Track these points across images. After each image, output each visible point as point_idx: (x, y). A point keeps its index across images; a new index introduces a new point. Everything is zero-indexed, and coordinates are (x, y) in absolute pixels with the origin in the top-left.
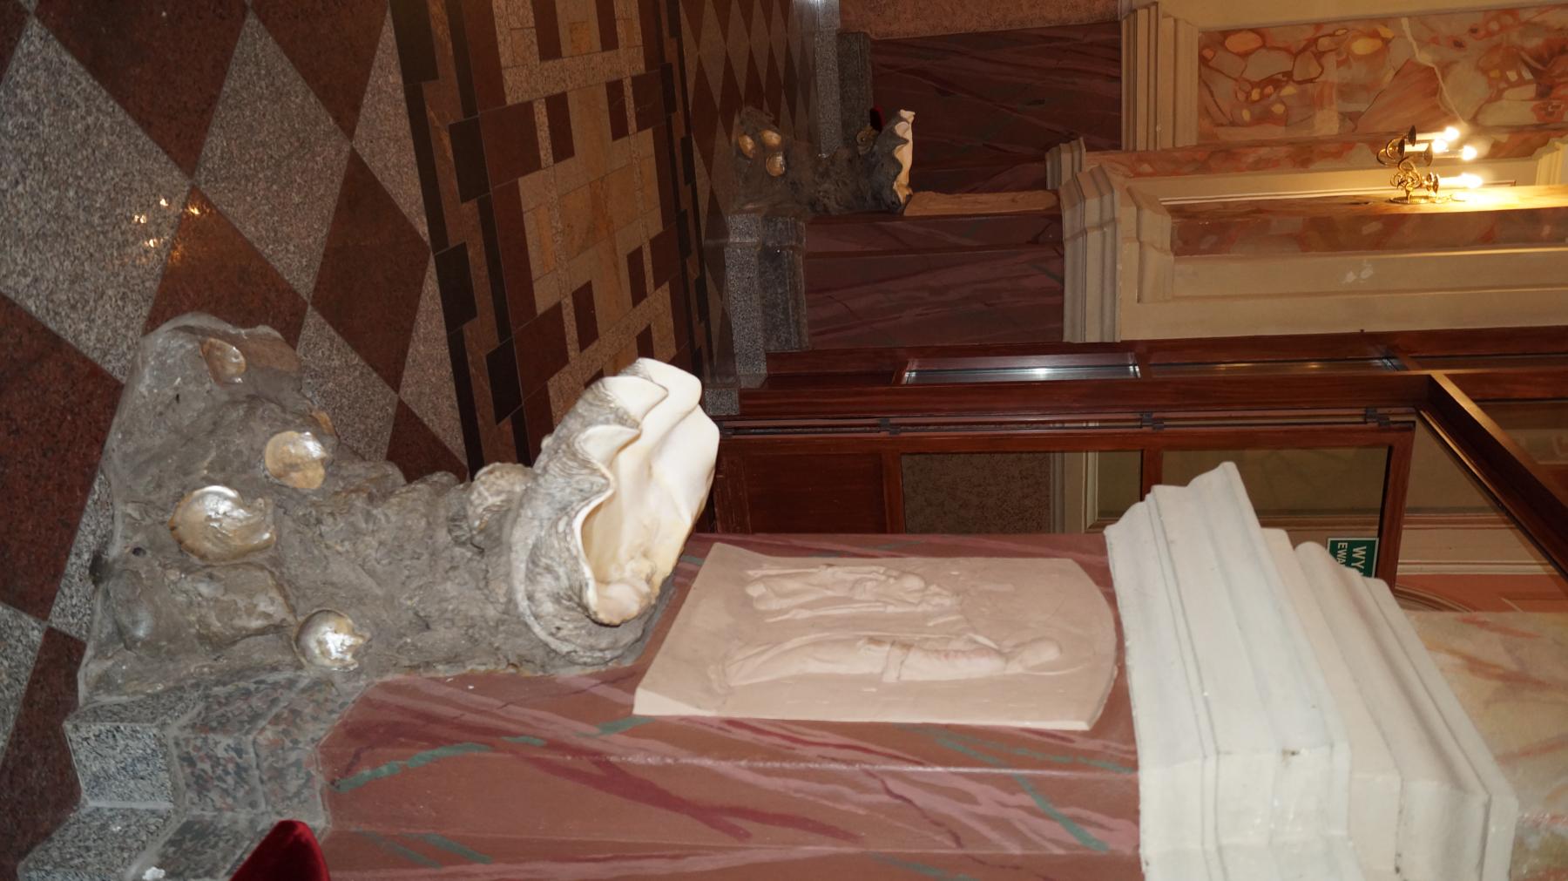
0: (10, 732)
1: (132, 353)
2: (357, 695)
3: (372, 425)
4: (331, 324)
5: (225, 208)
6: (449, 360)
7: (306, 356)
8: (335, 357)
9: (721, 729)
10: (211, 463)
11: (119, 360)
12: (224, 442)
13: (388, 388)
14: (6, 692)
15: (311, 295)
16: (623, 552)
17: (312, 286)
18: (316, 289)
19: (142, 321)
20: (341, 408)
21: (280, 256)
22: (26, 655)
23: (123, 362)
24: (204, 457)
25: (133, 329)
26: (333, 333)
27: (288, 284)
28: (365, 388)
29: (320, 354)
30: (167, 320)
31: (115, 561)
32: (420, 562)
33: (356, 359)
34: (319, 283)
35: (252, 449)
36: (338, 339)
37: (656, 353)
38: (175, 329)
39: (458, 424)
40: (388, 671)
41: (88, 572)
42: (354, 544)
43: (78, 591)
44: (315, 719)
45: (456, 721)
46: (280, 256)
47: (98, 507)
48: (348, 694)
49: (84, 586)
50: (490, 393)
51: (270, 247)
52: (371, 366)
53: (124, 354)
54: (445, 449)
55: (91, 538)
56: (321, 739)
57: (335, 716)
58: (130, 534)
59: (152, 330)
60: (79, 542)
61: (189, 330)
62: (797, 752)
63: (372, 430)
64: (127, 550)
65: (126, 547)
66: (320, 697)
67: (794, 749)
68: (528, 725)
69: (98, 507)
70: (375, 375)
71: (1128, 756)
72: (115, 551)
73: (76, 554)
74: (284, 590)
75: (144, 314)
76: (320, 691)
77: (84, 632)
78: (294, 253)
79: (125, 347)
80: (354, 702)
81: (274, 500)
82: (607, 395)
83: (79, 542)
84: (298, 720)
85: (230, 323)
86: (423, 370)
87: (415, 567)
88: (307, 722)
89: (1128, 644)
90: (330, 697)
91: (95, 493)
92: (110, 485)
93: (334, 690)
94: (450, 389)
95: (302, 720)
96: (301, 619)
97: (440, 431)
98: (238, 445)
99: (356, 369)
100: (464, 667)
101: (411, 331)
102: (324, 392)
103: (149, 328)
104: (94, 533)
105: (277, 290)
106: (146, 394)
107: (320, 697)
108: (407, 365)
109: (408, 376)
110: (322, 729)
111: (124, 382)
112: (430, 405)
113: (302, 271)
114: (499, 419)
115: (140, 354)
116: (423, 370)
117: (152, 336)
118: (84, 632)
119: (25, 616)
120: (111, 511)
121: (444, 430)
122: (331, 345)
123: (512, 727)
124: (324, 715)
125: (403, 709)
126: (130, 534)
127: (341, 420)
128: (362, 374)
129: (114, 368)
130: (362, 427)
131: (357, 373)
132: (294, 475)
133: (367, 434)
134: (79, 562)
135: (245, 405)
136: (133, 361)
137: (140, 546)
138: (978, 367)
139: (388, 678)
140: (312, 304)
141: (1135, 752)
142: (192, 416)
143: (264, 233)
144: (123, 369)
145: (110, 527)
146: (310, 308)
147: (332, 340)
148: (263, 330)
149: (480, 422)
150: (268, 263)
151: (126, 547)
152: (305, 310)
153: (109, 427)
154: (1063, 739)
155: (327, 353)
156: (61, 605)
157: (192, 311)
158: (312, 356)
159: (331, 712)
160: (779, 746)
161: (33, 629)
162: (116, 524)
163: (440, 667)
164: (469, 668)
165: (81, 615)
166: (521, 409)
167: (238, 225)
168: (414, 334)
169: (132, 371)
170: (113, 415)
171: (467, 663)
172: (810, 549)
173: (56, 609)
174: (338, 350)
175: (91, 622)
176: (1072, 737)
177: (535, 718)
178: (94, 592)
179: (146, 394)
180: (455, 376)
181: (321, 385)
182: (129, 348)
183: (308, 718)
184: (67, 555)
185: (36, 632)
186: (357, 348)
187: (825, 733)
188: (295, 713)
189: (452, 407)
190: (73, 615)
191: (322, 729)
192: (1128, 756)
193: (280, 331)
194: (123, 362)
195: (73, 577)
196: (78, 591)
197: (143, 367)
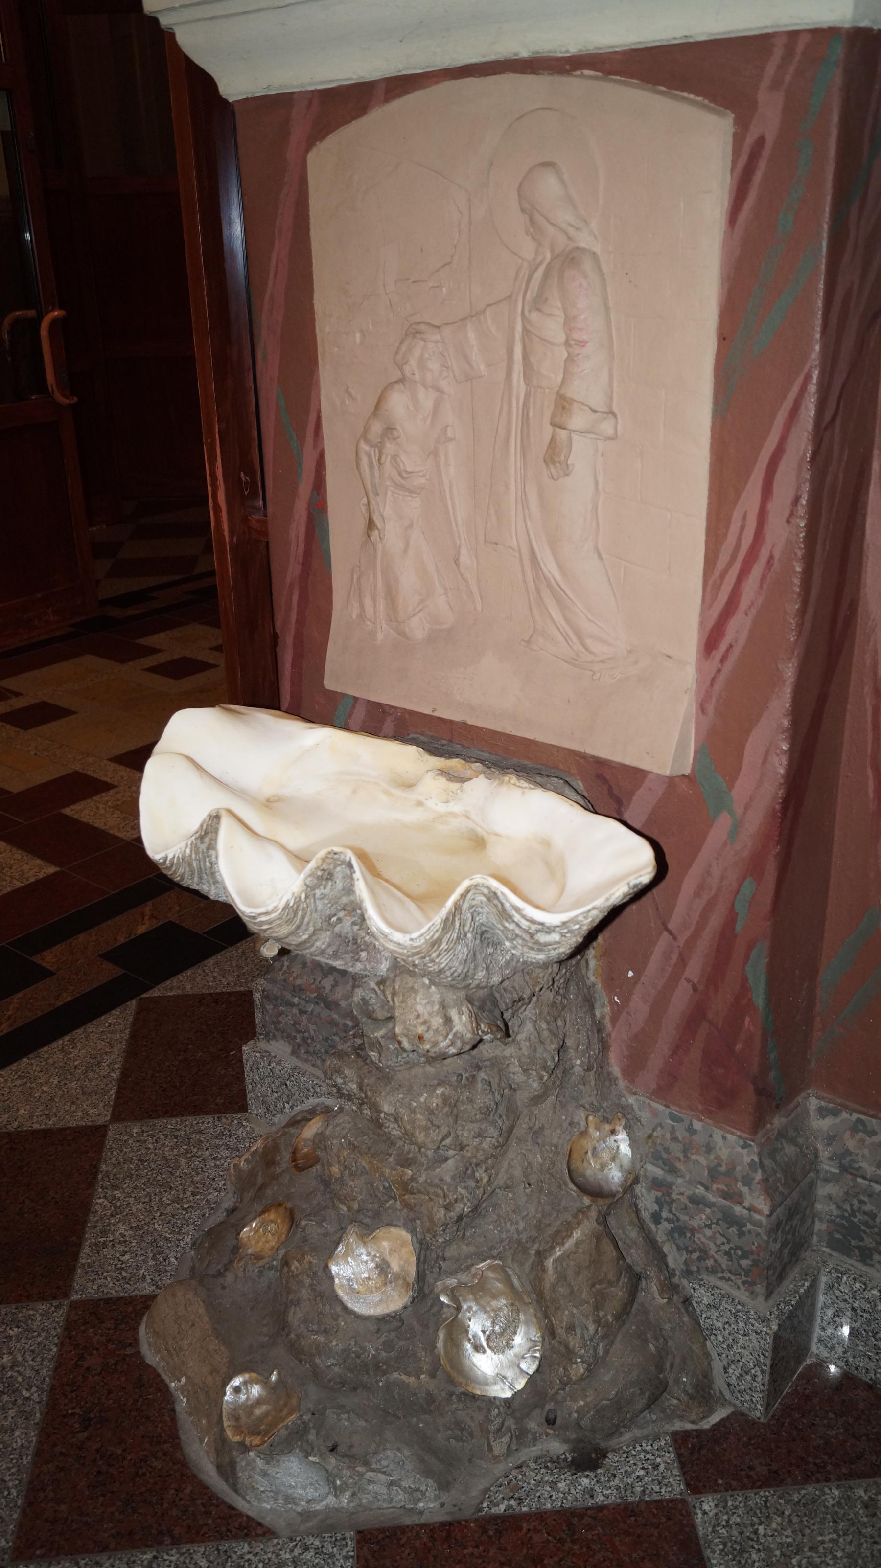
0: (818, 1486)
1: (310, 1540)
2: (654, 1105)
3: (172, 1149)
4: (76, 1256)
5: (14, 1492)
6: (14, 1067)
7: (144, 1277)
8: (117, 1234)
9: (723, 660)
10: (409, 1374)
11: (332, 1556)
12: (377, 1368)
13: (109, 1143)
14: (787, 1513)
15: (55, 1303)
16: (414, 816)
17: (42, 1307)
18: (42, 1298)
19: (259, 1546)
20: (178, 1200)
21: (28, 1373)
22: (736, 1508)
23: (329, 1548)
24: (403, 1385)
25: (278, 1555)
26: (86, 1250)
27: (62, 1344)
28: (130, 1176)
29: (127, 1257)
30: (232, 1508)
31: (566, 1441)
32: (492, 1080)
33: (100, 1203)
34: (29, 1298)
35: (378, 1330)
36: (90, 1237)
37: (135, 836)
38: (236, 1491)
39: (90, 1028)
40: (609, 1074)
41: (599, 1471)
42: (477, 1165)
43: (628, 1474)
44: (709, 1149)
45: (701, 988)
46: (28, 1373)
47: (521, 1493)
48: (655, 1113)
49: (616, 1468)
50: (20, 995)
51: (25, 1394)
52: (95, 1178)
53: (318, 1552)
54: (133, 1036)
55: (562, 1485)
56: (740, 1137)
57: (697, 1125)
58: (530, 1436)
59: (260, 1524)
60: (576, 1500)
61: (228, 1470)
62: (777, 554)
63: (176, 1146)
64: (551, 1431)
65: (547, 1435)
66: (676, 1149)
67: (771, 557)
68: (710, 906)
69: (521, 1493)
70: (104, 1167)
71: (800, 47)
72: (557, 1447)
73: (592, 1496)
74: (558, 1232)
75: (246, 1548)
76: (667, 1150)
77: (663, 1443)
78: (10, 1353)
79: (309, 1555)
80: (667, 1106)
81: (436, 1280)
82: (287, 906)
83: (576, 1500)
84: (723, 1169)
85: (173, 1410)
86: (52, 1099)
87: (499, 1085)
88: (718, 1157)
89: (524, 54)
90: (668, 1136)
91: (510, 1507)
92: (487, 1490)
93: (655, 1134)
94: (53, 1052)
95: (720, 1165)
96: (587, 1201)
97: (116, 1051)
98: (377, 1350)
99: (114, 1197)
100: (594, 985)
101: (9, 1134)
102: (173, 1232)
103: (260, 1531)
104: (553, 1485)
105: (82, 1357)
106: (348, 1494)
107: (676, 1149)
108: (60, 1125)
109: (75, 1119)
110: (724, 1138)
111: (351, 1534)
112: (91, 1075)
113: (29, 1330)
114: (47, 974)
115: (302, 1528)
116: (52, 1099)
117: (267, 1521)
118: (663, 1443)
119: (701, 1532)
120: (514, 1473)
121: (111, 1046)
122: (105, 1245)
123: (715, 921)
124: (699, 1139)
125: (679, 1048)
126: (530, 1436)
127: (193, 1194)
128: (115, 1187)
129: (346, 1558)
130: (183, 1162)
131: (118, 1193)
132: (395, 1267)
133: (187, 1151)
134: (597, 1489)
135: (317, 1360)
136: (318, 1533)
137: (543, 1420)
138: (244, 295)
139: (616, 1070)
140: (66, 1295)
141: (793, 35)
142: (349, 1419)
143: (12, 1413)
144: (340, 1543)
145: (533, 1465)
146: (75, 1297)
147: (98, 1247)
148: (152, 1358)
149: (67, 998)
150: (53, 1388)
151: (547, 1435)
152: (83, 1303)
153: (423, 1526)
154: (754, 156)
155: (120, 1248)
156: (656, 1488)
157: (195, 1476)
158: (138, 1268)
159: (691, 1130)
160: (763, 578)
161: (705, 1513)
162: (523, 1459)
163: (598, 1014)
164: (593, 979)
165: (649, 1456)
166: (8, 944)
167: (26, 1460)
168: (10, 1128)
169: (332, 1528)
170: (403, 1529)
171: (589, 983)
172: (308, 554)
173: (666, 1493)
174: (104, 1233)
175: (646, 1438)
176: (750, 140)
177: (697, 894)
178: (614, 1450)
179: (348, 1494)
180: (31, 1052)
181: (167, 1239)
182: (306, 1549)
183: (712, 1157)
184: (601, 1508)
185: (706, 1507)
186: (86, 1207)
187: (737, 515)
188: (714, 1173)
189: (73, 1041)
190: (656, 1467)
191: (724, 1138)
192: (800, 47)
193: (135, 1329)
194: (329, 1548)
195: (618, 1488)
196: (628, 1474)
197: (316, 1514)
